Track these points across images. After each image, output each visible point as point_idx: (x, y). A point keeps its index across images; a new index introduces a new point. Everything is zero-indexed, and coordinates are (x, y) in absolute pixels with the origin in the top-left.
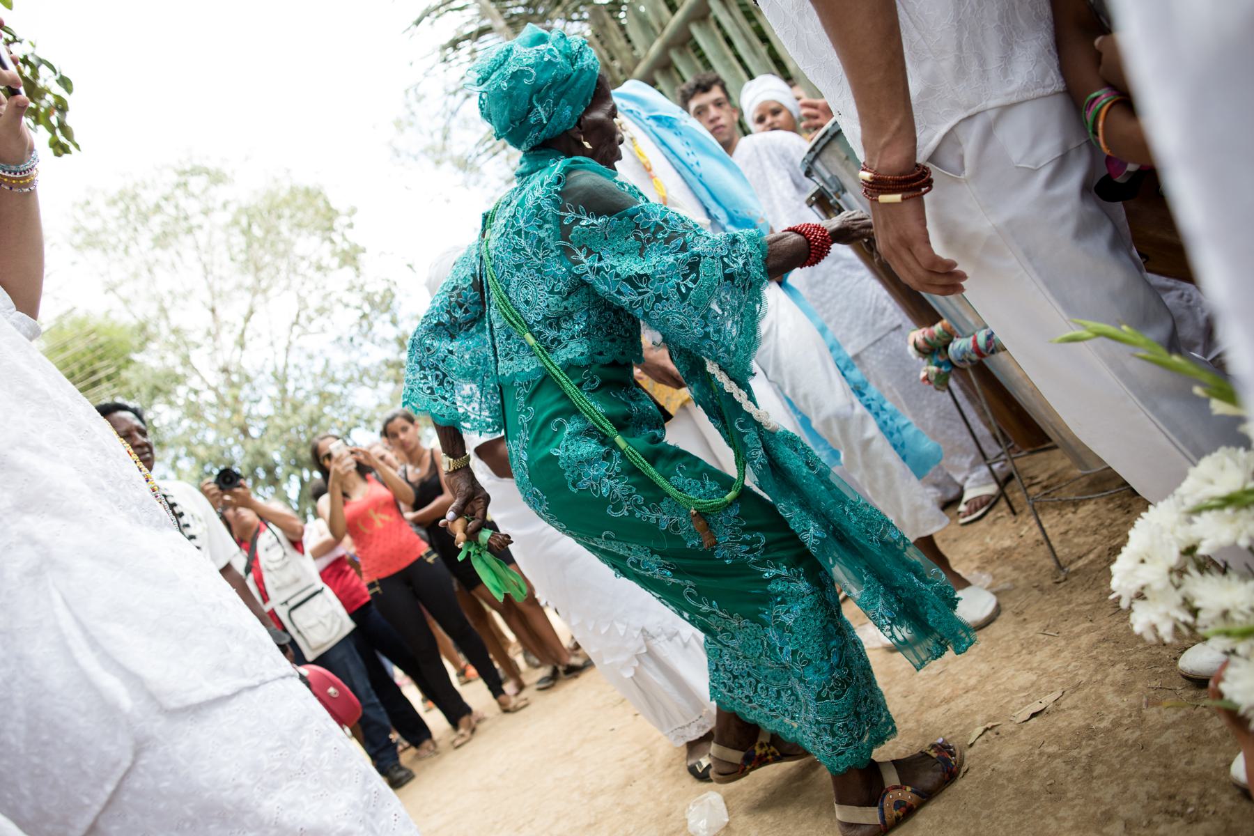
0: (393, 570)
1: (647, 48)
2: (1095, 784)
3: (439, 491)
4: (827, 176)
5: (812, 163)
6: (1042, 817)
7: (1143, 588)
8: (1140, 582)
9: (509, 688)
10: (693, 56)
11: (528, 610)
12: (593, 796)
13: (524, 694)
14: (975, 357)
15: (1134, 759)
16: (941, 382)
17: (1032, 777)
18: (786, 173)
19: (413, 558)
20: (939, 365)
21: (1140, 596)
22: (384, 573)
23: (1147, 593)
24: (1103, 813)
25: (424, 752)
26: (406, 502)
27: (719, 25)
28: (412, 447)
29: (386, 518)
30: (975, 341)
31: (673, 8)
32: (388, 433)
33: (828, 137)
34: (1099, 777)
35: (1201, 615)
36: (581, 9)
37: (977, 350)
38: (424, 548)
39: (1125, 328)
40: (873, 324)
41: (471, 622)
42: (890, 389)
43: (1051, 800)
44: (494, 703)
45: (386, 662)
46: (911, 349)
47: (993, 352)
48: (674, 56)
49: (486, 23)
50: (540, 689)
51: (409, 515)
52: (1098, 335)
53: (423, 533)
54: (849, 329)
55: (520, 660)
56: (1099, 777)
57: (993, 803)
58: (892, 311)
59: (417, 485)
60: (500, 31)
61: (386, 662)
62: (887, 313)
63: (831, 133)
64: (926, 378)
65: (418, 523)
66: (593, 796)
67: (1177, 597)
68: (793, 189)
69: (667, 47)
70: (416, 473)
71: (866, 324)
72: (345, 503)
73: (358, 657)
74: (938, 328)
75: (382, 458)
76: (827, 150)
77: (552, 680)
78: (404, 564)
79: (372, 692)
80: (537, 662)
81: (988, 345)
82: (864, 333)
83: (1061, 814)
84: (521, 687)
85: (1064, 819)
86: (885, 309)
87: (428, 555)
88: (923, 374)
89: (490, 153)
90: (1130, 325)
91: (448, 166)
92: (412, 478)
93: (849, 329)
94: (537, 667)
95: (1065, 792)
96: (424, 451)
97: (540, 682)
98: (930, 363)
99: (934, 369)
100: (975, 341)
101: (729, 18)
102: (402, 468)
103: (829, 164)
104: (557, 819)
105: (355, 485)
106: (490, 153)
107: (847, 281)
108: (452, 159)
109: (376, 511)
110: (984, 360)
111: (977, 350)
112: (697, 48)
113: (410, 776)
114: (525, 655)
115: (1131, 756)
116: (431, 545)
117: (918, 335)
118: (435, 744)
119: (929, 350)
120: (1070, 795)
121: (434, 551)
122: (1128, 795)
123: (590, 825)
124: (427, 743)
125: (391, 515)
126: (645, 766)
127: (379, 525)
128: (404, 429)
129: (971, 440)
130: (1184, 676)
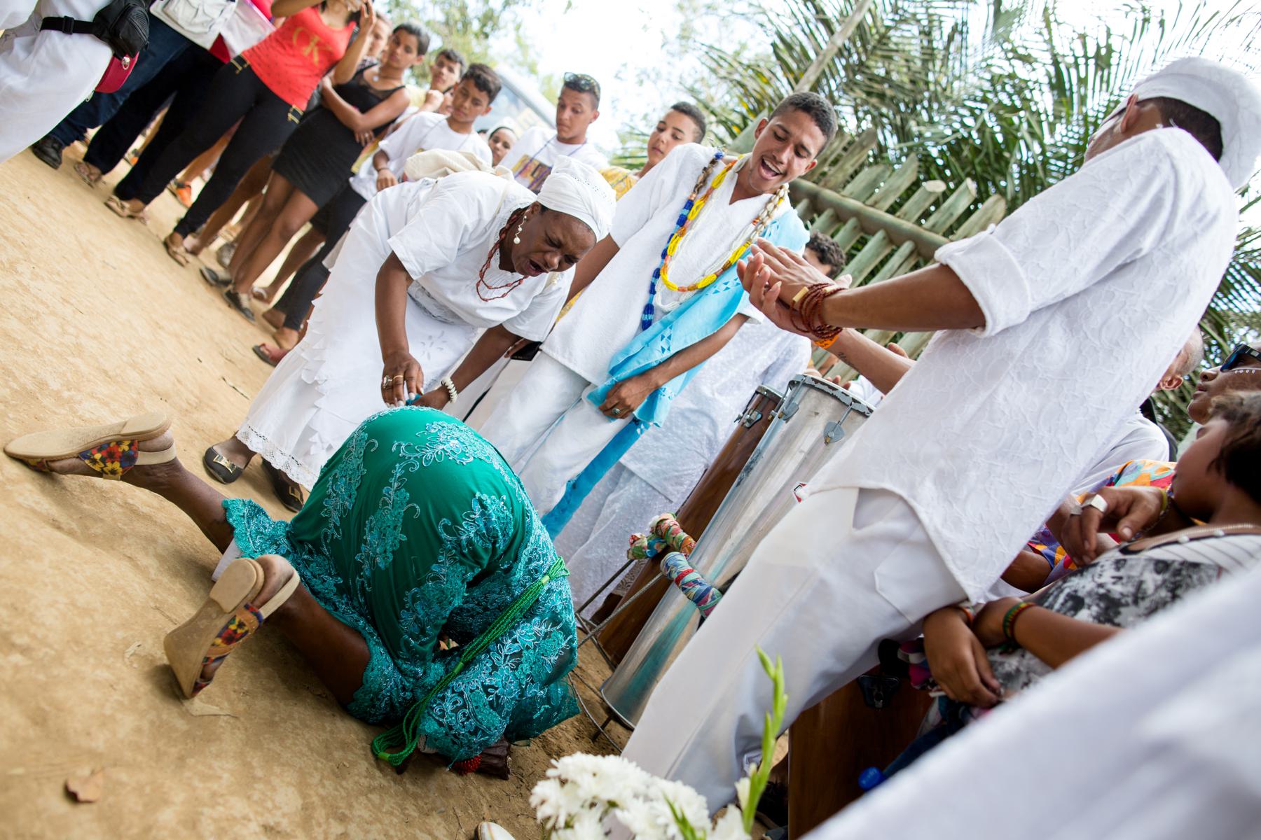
0: (267, 80)
1: (852, 196)
2: (362, 799)
3: (364, 109)
4: (796, 402)
5: (805, 384)
6: (316, 769)
7: (574, 782)
8: (578, 779)
9: (190, 241)
10: (853, 243)
11: (275, 234)
12: (134, 365)
13: (190, 258)
14: (675, 576)
15: (395, 820)
16: (636, 553)
17: (343, 749)
18: (775, 359)
19: (287, 97)
20: (650, 546)
21: (563, 782)
22: (258, 70)
23: (567, 786)
24: (343, 814)
25: (85, 169)
26: (336, 76)
27: (891, 255)
28: (395, 65)
29: (316, 59)
30: (688, 572)
31: (892, 210)
32: (403, 31)
33: (831, 392)
34: (369, 800)
35: (569, 831)
36: (869, 117)
37: (681, 576)
38: (300, 106)
39: (785, 697)
40: (665, 479)
41: (242, 181)
42: (614, 512)
43: (333, 771)
44: (171, 231)
45: (170, 100)
46: (657, 518)
47: (684, 589)
48: (851, 222)
49: (837, 27)
50: (202, 272)
51: (328, 82)
52: (775, 682)
53: (316, 102)
54: (655, 460)
55: (219, 242)
56: (369, 800)
57: (307, 726)
58: (681, 493)
59: (362, 83)
60: (833, 43)
61: (170, 100)
62: (679, 488)
63: (835, 393)
64: (635, 539)
65: (323, 94)
66: (134, 365)
67: (575, 809)
68: (763, 370)
69: (856, 214)
70: (372, 76)
71: (664, 472)
72: (315, 7)
73: (159, 69)
74: (683, 535)
75: (377, 37)
76: (819, 394)
77: (212, 280)
78: (276, 89)
79: (128, 95)
80: (227, 261)
81: (688, 584)
82: (656, 473)
83: (327, 783)
84: (195, 252)
85: (324, 786)
86: (681, 484)
87: (295, 113)
88: (638, 535)
89: (714, 65)
90: (789, 701)
91: (680, 18)
92: (367, 74)
93: (655, 460)
94: (220, 262)
95: (344, 778)
96: (399, 79)
97: (209, 270)
98: (649, 538)
99: (646, 544)
100: (688, 572)
101: (896, 266)
102: (375, 61)
103: (807, 399)
104: (95, 338)
105: (338, 13)
106: (714, 65)
107: (696, 444)
108: (688, 21)
109: (318, 44)
110: (674, 584)
111: (681, 576)
112: (863, 242)
113: (55, 163)
114: (229, 246)
115: (396, 817)
116: (306, 114)
117: (671, 521)
118: (98, 179)
119: (659, 532)
120: (344, 783)
121: (302, 119)
122: (366, 826)
123: (105, 372)
124: (96, 171)
125: (320, 62)
126: (185, 406)
127: (306, 51)
128: (408, 50)
129: (591, 594)
130: (476, 831)
